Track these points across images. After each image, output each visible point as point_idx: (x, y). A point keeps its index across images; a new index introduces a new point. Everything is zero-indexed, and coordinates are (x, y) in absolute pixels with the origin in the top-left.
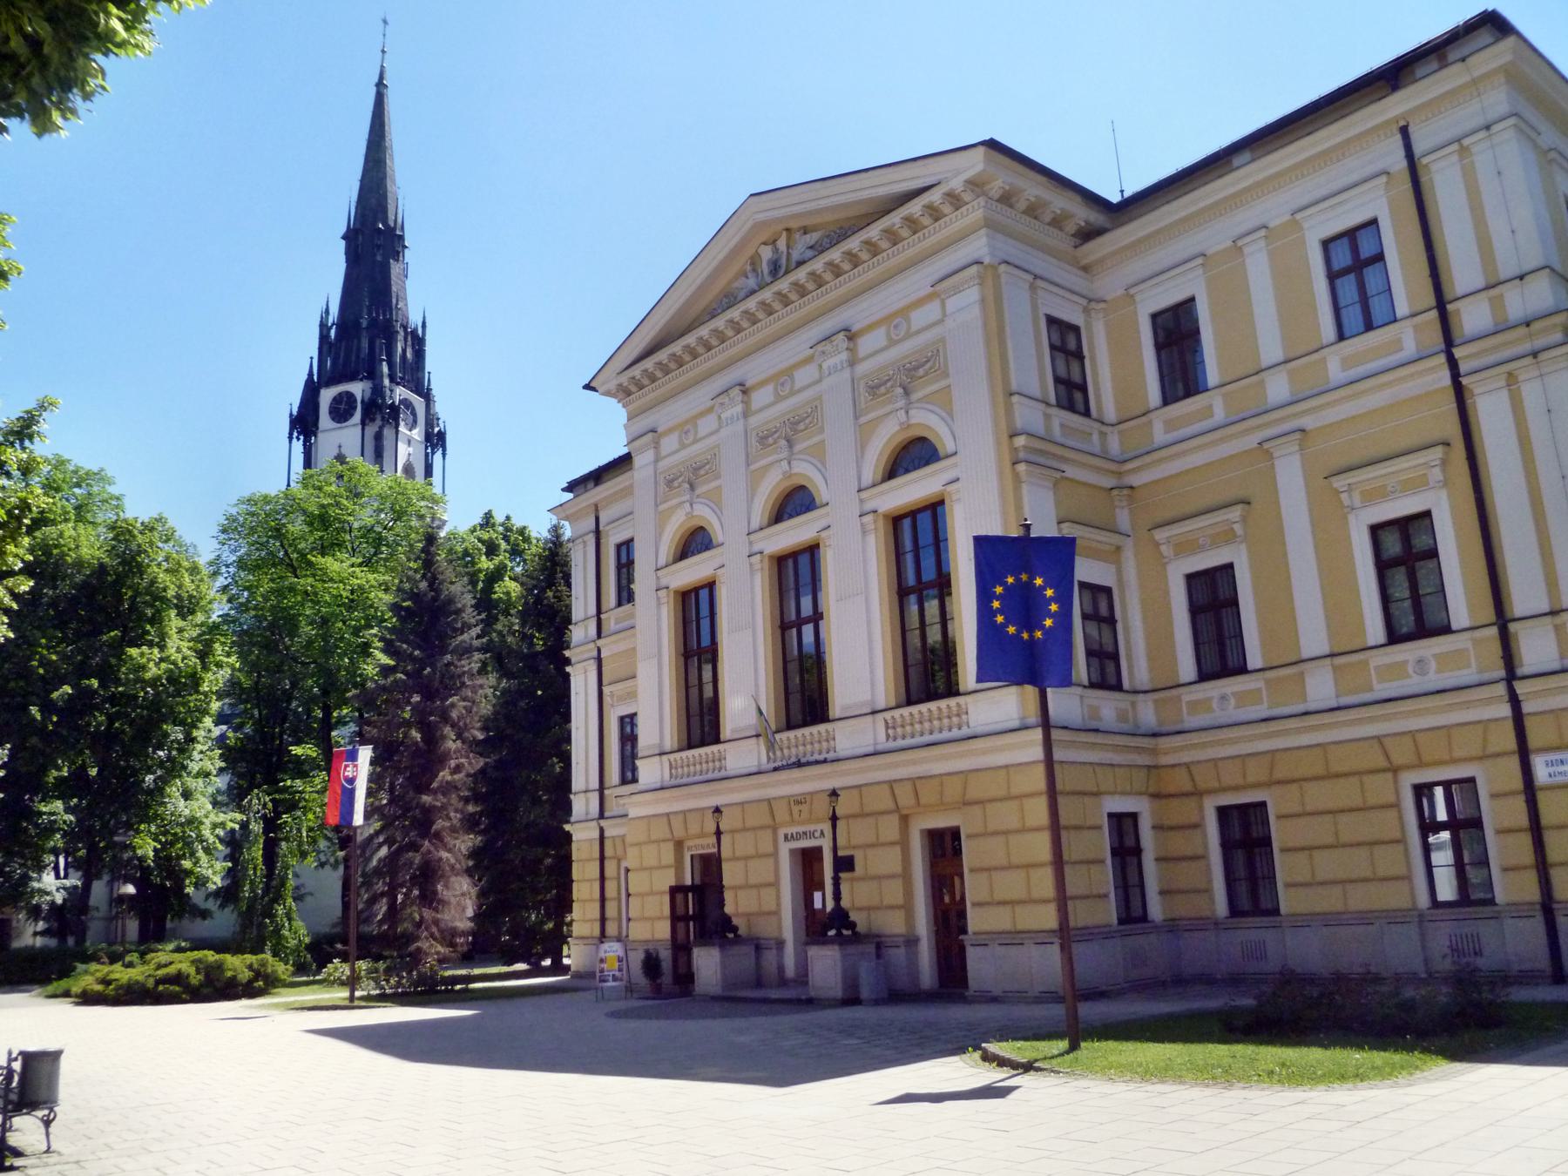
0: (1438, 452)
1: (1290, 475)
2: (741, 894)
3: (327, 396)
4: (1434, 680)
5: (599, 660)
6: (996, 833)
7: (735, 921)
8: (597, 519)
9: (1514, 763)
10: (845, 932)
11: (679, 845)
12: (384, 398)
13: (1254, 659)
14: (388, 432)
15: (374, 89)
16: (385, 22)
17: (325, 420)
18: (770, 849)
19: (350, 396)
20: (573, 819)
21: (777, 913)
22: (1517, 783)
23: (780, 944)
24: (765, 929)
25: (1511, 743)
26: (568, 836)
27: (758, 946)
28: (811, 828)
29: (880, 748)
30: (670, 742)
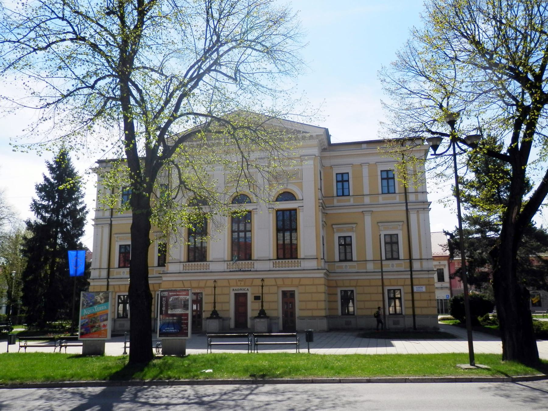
0: (402, 223)
1: (368, 219)
4: (395, 269)
5: (111, 225)
9: (410, 287)
13: (355, 258)
20: (91, 278)
22: (410, 291)
25: (409, 283)
26: (89, 284)
28: (244, 288)
29: (271, 269)
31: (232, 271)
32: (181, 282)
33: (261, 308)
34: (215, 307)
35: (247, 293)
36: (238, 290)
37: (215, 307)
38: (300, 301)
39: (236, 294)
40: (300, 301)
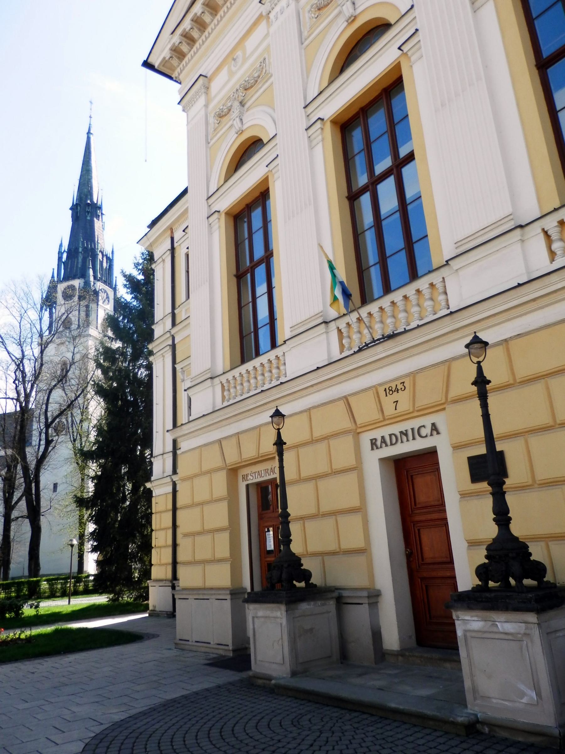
2: (311, 525)
3: (61, 287)
6: (163, 565)
7: (307, 564)
8: (172, 239)
10: (527, 582)
11: (233, 472)
12: (90, 286)
14: (93, 306)
15: (86, 136)
16: (91, 102)
17: (60, 299)
18: (351, 461)
19: (72, 287)
21: (364, 551)
23: (374, 596)
24: (347, 576)
27: (339, 598)
28: (415, 423)
30: (222, 360)
33: (492, 531)
36: (394, 439)
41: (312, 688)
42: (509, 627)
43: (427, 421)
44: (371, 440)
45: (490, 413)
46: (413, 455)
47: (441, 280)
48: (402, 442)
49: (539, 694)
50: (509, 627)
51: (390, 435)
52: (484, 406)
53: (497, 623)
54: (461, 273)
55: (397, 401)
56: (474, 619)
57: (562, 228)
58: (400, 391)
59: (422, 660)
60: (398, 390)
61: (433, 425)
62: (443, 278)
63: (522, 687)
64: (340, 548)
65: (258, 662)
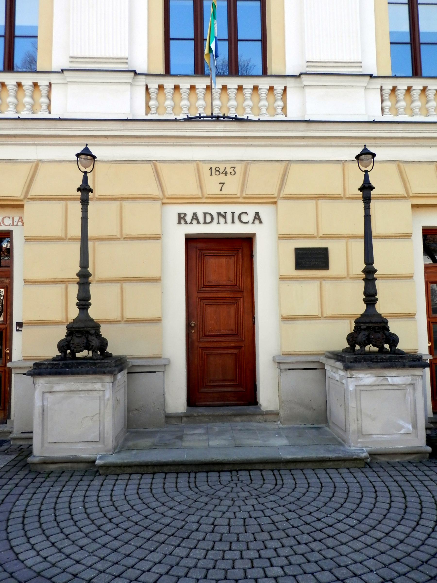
23: (356, 357)
28: (238, 209)
31: (200, 119)
32: (149, 168)
33: (74, 313)
34: (84, 303)
35: (12, 231)
37: (84, 303)
38: (27, 282)
39: (191, 241)
40: (27, 282)
41: (150, 460)
42: (398, 380)
43: (252, 210)
44: (179, 214)
45: (371, 214)
46: (235, 237)
47: (48, 84)
48: (218, 223)
49: (415, 426)
50: (398, 380)
51: (205, 214)
52: (367, 209)
53: (388, 378)
54: (307, 90)
55: (224, 183)
56: (367, 376)
57: (34, 88)
58: (228, 175)
59: (211, 417)
60: (226, 174)
61: (257, 214)
62: (50, 84)
63: (401, 422)
64: (122, 317)
65: (46, 445)
